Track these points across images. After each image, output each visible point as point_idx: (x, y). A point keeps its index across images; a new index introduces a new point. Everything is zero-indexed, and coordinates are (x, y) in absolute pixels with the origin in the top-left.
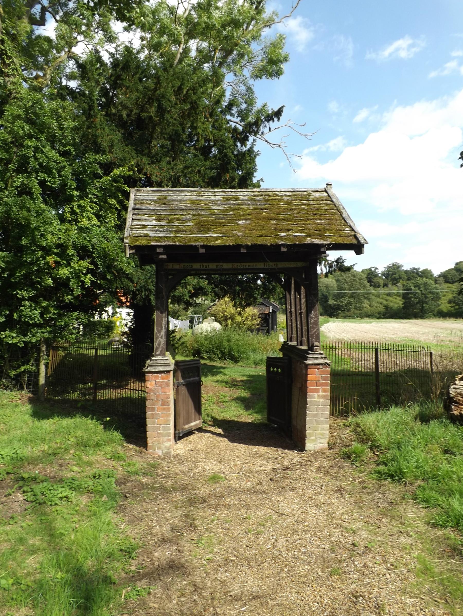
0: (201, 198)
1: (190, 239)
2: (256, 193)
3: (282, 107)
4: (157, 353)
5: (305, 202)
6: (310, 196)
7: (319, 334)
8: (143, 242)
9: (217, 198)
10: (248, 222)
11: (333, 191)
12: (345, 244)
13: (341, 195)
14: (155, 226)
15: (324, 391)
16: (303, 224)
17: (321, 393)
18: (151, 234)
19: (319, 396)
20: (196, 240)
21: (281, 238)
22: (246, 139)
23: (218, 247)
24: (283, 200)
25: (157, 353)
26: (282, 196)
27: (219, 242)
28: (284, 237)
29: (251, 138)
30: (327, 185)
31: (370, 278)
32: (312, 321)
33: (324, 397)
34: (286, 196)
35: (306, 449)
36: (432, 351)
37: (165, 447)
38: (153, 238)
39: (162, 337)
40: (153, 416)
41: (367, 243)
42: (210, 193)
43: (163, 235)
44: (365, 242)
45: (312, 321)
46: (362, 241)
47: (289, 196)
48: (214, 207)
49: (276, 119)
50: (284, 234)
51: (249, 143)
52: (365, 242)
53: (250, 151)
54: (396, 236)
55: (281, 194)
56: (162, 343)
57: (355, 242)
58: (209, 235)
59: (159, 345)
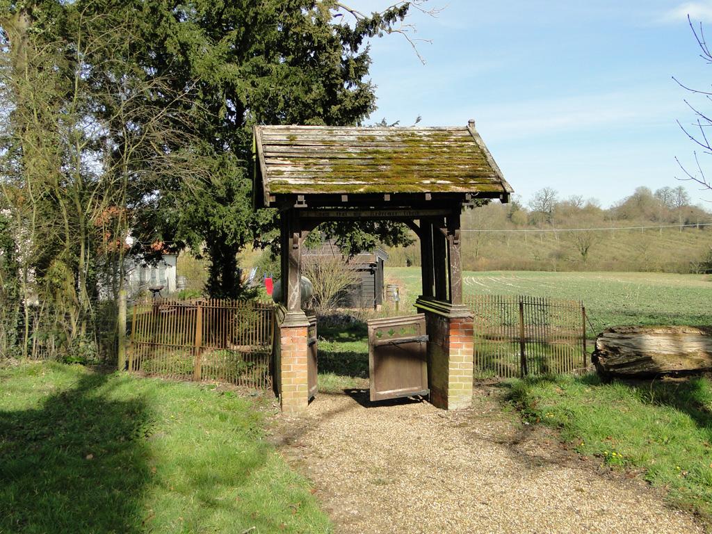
0: (334, 139)
1: (332, 187)
2: (393, 132)
3: (408, 4)
4: (292, 308)
5: (446, 143)
6: (451, 135)
7: (461, 285)
8: (283, 190)
9: (352, 138)
10: (389, 167)
11: (477, 129)
12: (490, 193)
13: (488, 138)
14: (292, 172)
15: (468, 346)
16: (447, 170)
17: (464, 348)
18: (291, 181)
19: (462, 352)
20: (339, 187)
21: (425, 186)
22: (359, 40)
23: (361, 195)
24: (422, 140)
25: (292, 308)
26: (420, 136)
27: (362, 190)
28: (425, 186)
29: (365, 39)
30: (469, 122)
31: (205, 465)
32: (455, 272)
33: (468, 353)
34: (426, 136)
35: (449, 408)
36: (585, 305)
37: (302, 408)
38: (294, 186)
39: (296, 291)
40: (289, 375)
41: (513, 192)
42: (343, 133)
43: (303, 182)
44: (510, 190)
45: (455, 272)
46: (508, 190)
47: (429, 136)
48: (350, 150)
49: (398, 18)
50: (428, 182)
51: (361, 49)
52: (510, 190)
53: (364, 57)
54: (563, 150)
55: (419, 134)
56: (296, 297)
57: (501, 189)
58: (351, 183)
59: (293, 299)
